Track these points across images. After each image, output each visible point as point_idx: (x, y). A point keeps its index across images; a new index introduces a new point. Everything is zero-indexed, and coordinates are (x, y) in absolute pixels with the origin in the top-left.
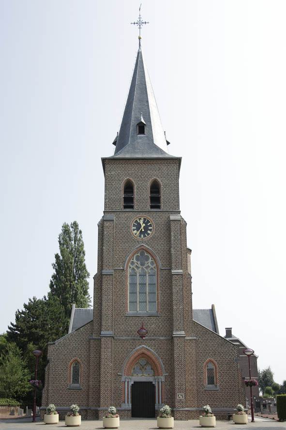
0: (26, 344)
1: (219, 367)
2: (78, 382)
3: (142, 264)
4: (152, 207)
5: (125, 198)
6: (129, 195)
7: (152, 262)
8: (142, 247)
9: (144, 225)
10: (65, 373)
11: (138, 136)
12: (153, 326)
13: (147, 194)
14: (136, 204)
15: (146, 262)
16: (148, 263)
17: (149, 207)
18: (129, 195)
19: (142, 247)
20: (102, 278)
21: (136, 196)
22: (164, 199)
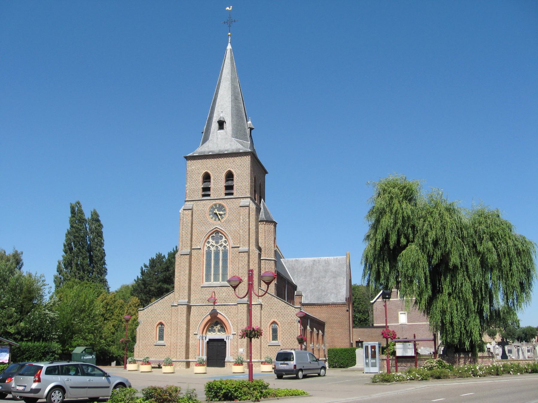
0: (355, 349)
1: (281, 326)
2: (163, 340)
3: (217, 243)
4: (226, 194)
5: (225, 186)
6: (230, 183)
7: (225, 241)
8: (217, 229)
9: (216, 210)
10: (152, 333)
11: (218, 131)
12: (224, 294)
13: (222, 183)
14: (211, 192)
15: (220, 241)
16: (221, 242)
17: (200, 196)
18: (230, 183)
19: (217, 229)
20: (260, 261)
21: (212, 185)
22: (237, 187)
